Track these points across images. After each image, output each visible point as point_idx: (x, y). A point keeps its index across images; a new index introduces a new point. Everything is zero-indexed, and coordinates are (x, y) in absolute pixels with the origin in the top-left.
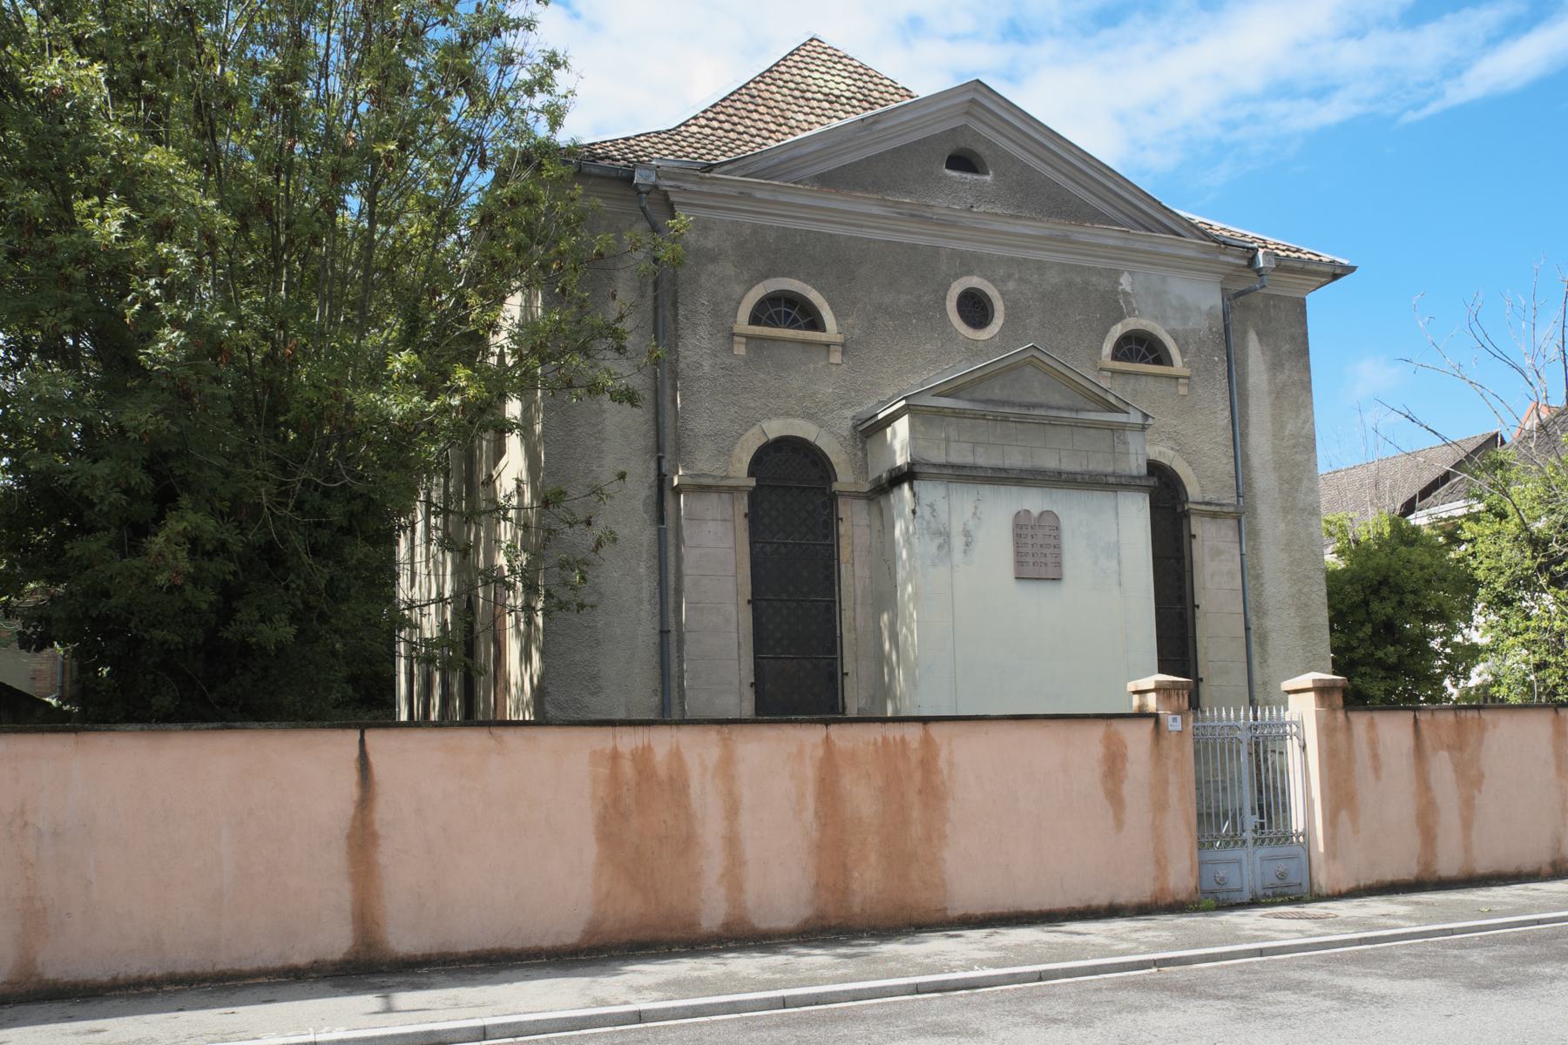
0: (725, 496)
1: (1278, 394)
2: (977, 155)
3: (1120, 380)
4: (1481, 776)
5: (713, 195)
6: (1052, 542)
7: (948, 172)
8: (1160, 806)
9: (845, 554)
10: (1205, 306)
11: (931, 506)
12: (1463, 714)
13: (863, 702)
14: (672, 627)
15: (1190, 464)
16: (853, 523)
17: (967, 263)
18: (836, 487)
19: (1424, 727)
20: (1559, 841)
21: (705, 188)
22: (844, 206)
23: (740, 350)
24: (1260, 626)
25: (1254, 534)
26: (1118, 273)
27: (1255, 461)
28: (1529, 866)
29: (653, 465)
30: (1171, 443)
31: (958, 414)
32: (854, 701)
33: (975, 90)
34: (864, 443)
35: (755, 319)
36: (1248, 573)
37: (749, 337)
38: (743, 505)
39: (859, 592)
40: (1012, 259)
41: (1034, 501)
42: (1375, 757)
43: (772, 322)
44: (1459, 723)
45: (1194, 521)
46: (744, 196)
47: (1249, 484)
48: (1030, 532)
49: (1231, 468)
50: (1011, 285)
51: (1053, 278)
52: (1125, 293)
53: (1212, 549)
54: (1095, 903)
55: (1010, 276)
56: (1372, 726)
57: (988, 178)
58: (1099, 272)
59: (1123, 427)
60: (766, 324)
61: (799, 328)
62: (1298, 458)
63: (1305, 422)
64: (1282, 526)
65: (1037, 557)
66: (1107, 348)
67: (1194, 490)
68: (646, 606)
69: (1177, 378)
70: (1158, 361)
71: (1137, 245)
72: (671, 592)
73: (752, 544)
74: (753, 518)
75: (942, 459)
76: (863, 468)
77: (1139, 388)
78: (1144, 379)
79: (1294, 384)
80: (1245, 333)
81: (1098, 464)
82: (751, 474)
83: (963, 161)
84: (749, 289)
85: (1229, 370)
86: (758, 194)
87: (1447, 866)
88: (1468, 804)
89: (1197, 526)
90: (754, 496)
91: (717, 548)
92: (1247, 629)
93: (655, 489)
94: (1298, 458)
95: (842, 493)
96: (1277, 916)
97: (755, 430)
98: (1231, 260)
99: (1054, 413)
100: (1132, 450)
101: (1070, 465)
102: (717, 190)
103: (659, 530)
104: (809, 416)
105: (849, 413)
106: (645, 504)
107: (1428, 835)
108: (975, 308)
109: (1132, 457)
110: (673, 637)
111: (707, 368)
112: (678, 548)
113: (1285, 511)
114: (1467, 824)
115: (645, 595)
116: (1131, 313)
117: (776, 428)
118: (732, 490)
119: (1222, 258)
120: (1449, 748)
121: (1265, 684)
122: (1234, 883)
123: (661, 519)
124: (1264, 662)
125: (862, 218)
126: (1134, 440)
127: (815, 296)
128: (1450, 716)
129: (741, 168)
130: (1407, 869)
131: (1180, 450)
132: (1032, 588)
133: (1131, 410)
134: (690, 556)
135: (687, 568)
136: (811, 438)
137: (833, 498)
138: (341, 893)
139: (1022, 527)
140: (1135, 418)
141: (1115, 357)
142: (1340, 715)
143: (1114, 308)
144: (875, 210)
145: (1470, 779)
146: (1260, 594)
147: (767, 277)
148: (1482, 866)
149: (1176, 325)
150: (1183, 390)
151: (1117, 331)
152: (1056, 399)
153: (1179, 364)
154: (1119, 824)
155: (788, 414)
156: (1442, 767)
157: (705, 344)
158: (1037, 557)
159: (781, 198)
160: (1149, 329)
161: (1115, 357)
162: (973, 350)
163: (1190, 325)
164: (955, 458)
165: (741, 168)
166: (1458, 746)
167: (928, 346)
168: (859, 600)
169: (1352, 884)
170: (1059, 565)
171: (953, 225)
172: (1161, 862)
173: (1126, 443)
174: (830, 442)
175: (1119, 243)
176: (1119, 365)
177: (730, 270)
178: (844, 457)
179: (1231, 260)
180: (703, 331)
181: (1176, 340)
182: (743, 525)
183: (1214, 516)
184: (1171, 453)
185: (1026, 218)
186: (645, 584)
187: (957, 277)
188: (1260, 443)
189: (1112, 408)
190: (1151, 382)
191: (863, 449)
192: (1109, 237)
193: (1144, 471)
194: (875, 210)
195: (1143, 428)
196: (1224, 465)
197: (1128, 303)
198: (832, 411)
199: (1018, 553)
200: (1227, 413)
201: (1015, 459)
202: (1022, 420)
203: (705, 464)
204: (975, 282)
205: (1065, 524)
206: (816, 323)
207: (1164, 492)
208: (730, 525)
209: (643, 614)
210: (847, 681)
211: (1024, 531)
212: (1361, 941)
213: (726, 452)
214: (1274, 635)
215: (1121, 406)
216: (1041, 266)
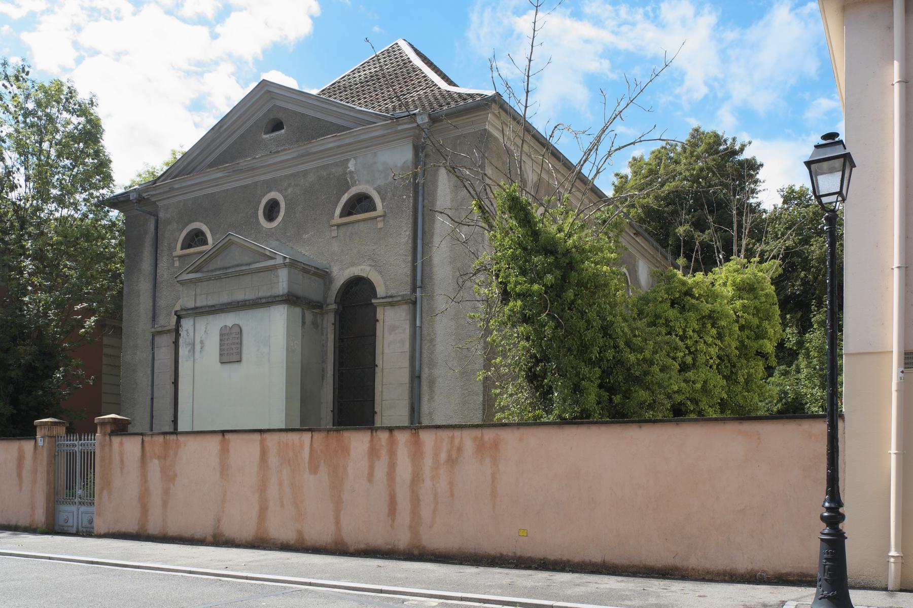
4: (176, 475)
5: (160, 194)
8: (34, 482)
11: (187, 331)
12: (168, 437)
15: (380, 273)
17: (269, 185)
19: (146, 445)
20: (219, 521)
21: (158, 192)
22: (207, 178)
26: (348, 160)
28: (198, 534)
30: (370, 262)
31: (199, 280)
40: (292, 175)
41: (230, 319)
42: (122, 461)
43: (190, 246)
44: (165, 442)
46: (172, 190)
51: (311, 178)
52: (351, 172)
54: (19, 524)
55: (289, 185)
56: (121, 444)
57: (283, 131)
58: (336, 164)
65: (231, 351)
67: (381, 291)
71: (347, 141)
78: (357, 225)
81: (264, 292)
83: (277, 126)
86: (176, 186)
87: (152, 529)
88: (166, 492)
96: (518, 576)
98: (406, 126)
99: (238, 269)
100: (281, 280)
101: (250, 295)
102: (161, 191)
107: (145, 510)
109: (280, 284)
112: (421, 344)
114: (165, 504)
119: (400, 128)
120: (159, 458)
121: (430, 413)
122: (70, 523)
125: (217, 182)
128: (161, 439)
129: (168, 177)
130: (133, 528)
131: (375, 265)
132: (228, 366)
133: (277, 257)
138: (254, 513)
139: (224, 334)
142: (107, 438)
144: (219, 175)
145: (169, 477)
146: (432, 353)
148: (172, 531)
149: (380, 182)
150: (380, 225)
152: (246, 259)
154: (20, 489)
156: (154, 466)
158: (231, 351)
159: (184, 184)
160: (364, 191)
165: (168, 177)
166: (163, 457)
169: (106, 531)
171: (253, 169)
172: (33, 508)
173: (278, 277)
175: (336, 144)
179: (406, 126)
180: (165, 259)
181: (379, 193)
183: (392, 304)
184: (368, 268)
185: (282, 151)
190: (361, 225)
192: (328, 142)
194: (219, 175)
197: (352, 178)
201: (225, 298)
202: (227, 276)
212: (462, 599)
214: (440, 380)
215: (272, 255)
216: (305, 173)
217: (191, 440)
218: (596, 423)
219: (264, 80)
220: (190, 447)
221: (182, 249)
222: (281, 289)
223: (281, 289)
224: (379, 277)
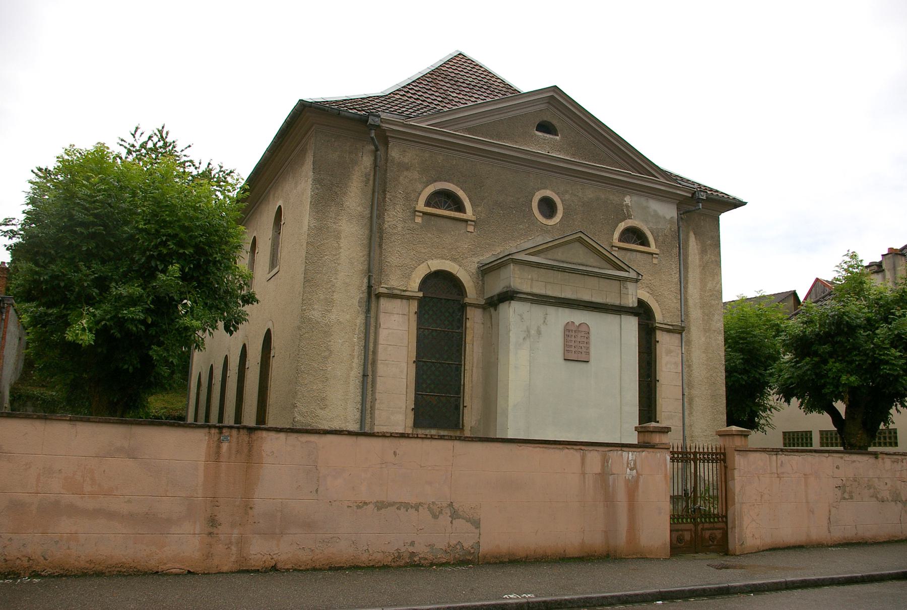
0: (405, 301)
1: (704, 267)
2: (303, 164)
3: (623, 252)
6: (585, 340)
7: (537, 133)
9: (469, 338)
10: (668, 217)
13: (473, 423)
14: (370, 373)
16: (475, 320)
18: (467, 300)
23: (419, 220)
24: (689, 394)
25: (689, 342)
27: (691, 302)
29: (366, 280)
31: (538, 265)
32: (471, 419)
33: (554, 91)
34: (483, 277)
35: (428, 204)
36: (686, 364)
37: (424, 213)
38: (414, 306)
39: (475, 360)
41: (578, 317)
45: (658, 333)
47: (687, 315)
48: (573, 334)
49: (678, 305)
50: (567, 197)
52: (627, 206)
53: (665, 343)
55: (567, 192)
57: (558, 138)
59: (626, 279)
60: (434, 207)
61: (451, 210)
62: (713, 302)
63: (717, 283)
64: (703, 339)
65: (576, 350)
66: (616, 235)
67: (658, 317)
68: (356, 360)
69: (652, 254)
70: (642, 244)
72: (371, 353)
73: (418, 329)
74: (420, 314)
75: (528, 290)
76: (481, 290)
77: (635, 260)
79: (712, 262)
80: (688, 233)
82: (420, 290)
84: (426, 187)
85: (679, 253)
89: (660, 336)
90: (422, 302)
91: (398, 329)
92: (683, 395)
93: (366, 295)
94: (713, 302)
95: (471, 305)
97: (423, 265)
100: (630, 292)
103: (366, 317)
104: (454, 260)
105: (476, 260)
106: (359, 302)
108: (548, 207)
109: (630, 297)
110: (370, 379)
111: (399, 229)
113: (705, 331)
115: (356, 354)
116: (629, 217)
117: (436, 265)
118: (409, 298)
123: (368, 311)
124: (691, 414)
126: (631, 286)
127: (461, 194)
134: (383, 334)
135: (381, 340)
136: (454, 272)
137: (463, 307)
139: (569, 331)
140: (633, 275)
141: (620, 240)
143: (622, 213)
147: (436, 181)
151: (622, 226)
153: (653, 248)
155: (442, 258)
157: (400, 215)
158: (576, 350)
160: (639, 226)
161: (620, 240)
162: (545, 229)
163: (660, 226)
164: (536, 290)
167: (521, 226)
168: (475, 365)
170: (588, 353)
174: (465, 275)
176: (622, 245)
177: (416, 175)
178: (471, 284)
182: (414, 318)
186: (356, 348)
187: (538, 190)
188: (693, 291)
189: (621, 269)
190: (639, 255)
191: (483, 280)
193: (636, 305)
195: (637, 281)
196: (673, 303)
197: (628, 211)
198: (467, 258)
199: (565, 345)
200: (677, 275)
201: (568, 294)
203: (394, 281)
204: (548, 193)
205: (593, 331)
206: (460, 208)
207: (643, 312)
208: (406, 317)
209: (354, 365)
210: (466, 410)
211: (571, 333)
213: (408, 277)
217: (273, 435)
218: (816, 451)
219: (460, 62)
220: (272, 444)
221: (648, 245)
222: (631, 301)
223: (631, 301)
224: (657, 305)
